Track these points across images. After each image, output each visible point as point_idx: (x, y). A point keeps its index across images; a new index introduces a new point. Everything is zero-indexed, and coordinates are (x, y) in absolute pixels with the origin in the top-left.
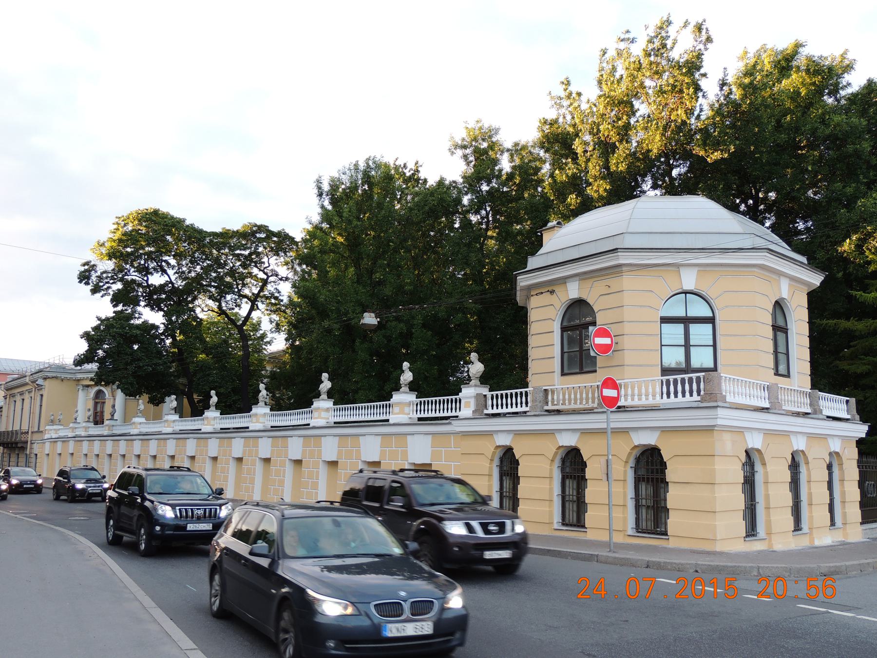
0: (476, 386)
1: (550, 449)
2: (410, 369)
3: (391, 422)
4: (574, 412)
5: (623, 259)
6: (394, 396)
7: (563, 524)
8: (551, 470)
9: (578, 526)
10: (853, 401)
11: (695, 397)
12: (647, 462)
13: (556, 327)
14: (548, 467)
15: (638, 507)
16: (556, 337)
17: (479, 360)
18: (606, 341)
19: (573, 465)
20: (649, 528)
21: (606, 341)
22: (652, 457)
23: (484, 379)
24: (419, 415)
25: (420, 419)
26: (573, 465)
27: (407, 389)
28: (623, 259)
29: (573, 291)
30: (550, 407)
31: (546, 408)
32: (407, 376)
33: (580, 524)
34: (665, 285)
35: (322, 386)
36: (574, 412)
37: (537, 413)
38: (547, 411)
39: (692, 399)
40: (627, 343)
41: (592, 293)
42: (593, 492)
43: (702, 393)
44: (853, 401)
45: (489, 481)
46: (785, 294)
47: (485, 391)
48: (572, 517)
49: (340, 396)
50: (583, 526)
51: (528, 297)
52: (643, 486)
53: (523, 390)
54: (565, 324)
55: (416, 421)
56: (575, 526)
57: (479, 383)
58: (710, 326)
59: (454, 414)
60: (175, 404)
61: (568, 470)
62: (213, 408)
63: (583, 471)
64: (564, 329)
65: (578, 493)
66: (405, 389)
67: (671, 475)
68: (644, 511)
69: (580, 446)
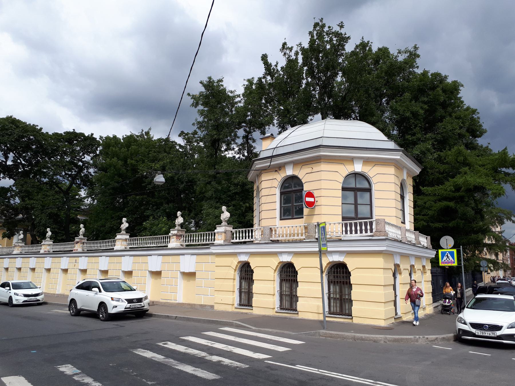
0: (225, 226)
1: (274, 262)
2: (182, 216)
3: (115, 249)
4: (289, 242)
5: (323, 153)
6: (217, 228)
7: (281, 309)
8: (234, 275)
9: (249, 306)
10: (429, 237)
11: (369, 233)
12: (334, 272)
13: (278, 192)
14: (273, 274)
15: (240, 293)
16: (277, 198)
17: (227, 211)
18: (312, 200)
19: (288, 273)
20: (287, 307)
21: (312, 200)
22: (337, 269)
23: (127, 230)
24: (187, 244)
25: (187, 246)
26: (288, 273)
27: (124, 232)
28: (323, 153)
29: (289, 172)
30: (273, 238)
31: (271, 239)
32: (125, 225)
33: (293, 308)
34: (345, 170)
35: (122, 226)
36: (289, 242)
37: (267, 242)
38: (232, 243)
39: (367, 234)
40: (320, 201)
41: (301, 173)
42: (301, 290)
43: (374, 231)
44: (429, 237)
45: (233, 282)
46: (405, 178)
47: (230, 229)
48: (287, 304)
49: (56, 239)
50: (251, 306)
51: (259, 176)
52: (284, 284)
53: (250, 229)
54: (282, 190)
55: (185, 247)
56: (247, 306)
57: (226, 224)
58: (368, 194)
59: (210, 242)
60: (22, 236)
61: (243, 275)
62: (48, 239)
63: (252, 275)
64: (282, 194)
65: (249, 287)
66: (48, 239)
67: (300, 278)
68: (284, 297)
69: (249, 261)
